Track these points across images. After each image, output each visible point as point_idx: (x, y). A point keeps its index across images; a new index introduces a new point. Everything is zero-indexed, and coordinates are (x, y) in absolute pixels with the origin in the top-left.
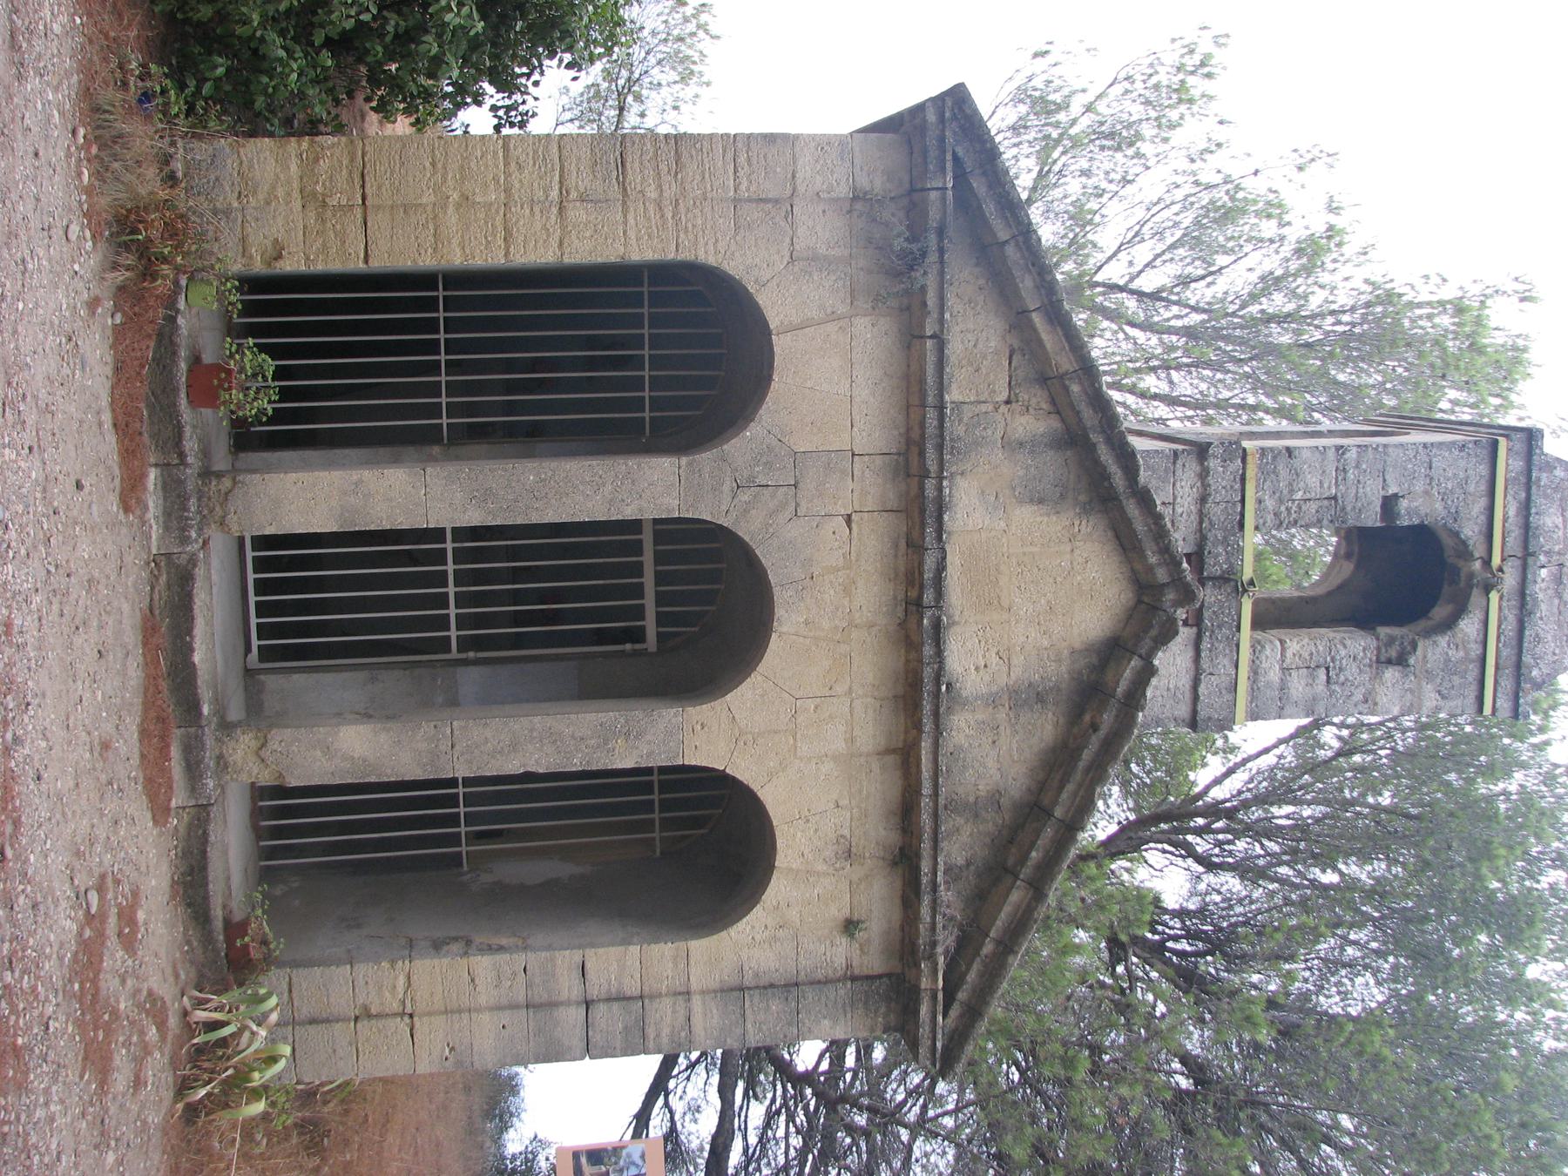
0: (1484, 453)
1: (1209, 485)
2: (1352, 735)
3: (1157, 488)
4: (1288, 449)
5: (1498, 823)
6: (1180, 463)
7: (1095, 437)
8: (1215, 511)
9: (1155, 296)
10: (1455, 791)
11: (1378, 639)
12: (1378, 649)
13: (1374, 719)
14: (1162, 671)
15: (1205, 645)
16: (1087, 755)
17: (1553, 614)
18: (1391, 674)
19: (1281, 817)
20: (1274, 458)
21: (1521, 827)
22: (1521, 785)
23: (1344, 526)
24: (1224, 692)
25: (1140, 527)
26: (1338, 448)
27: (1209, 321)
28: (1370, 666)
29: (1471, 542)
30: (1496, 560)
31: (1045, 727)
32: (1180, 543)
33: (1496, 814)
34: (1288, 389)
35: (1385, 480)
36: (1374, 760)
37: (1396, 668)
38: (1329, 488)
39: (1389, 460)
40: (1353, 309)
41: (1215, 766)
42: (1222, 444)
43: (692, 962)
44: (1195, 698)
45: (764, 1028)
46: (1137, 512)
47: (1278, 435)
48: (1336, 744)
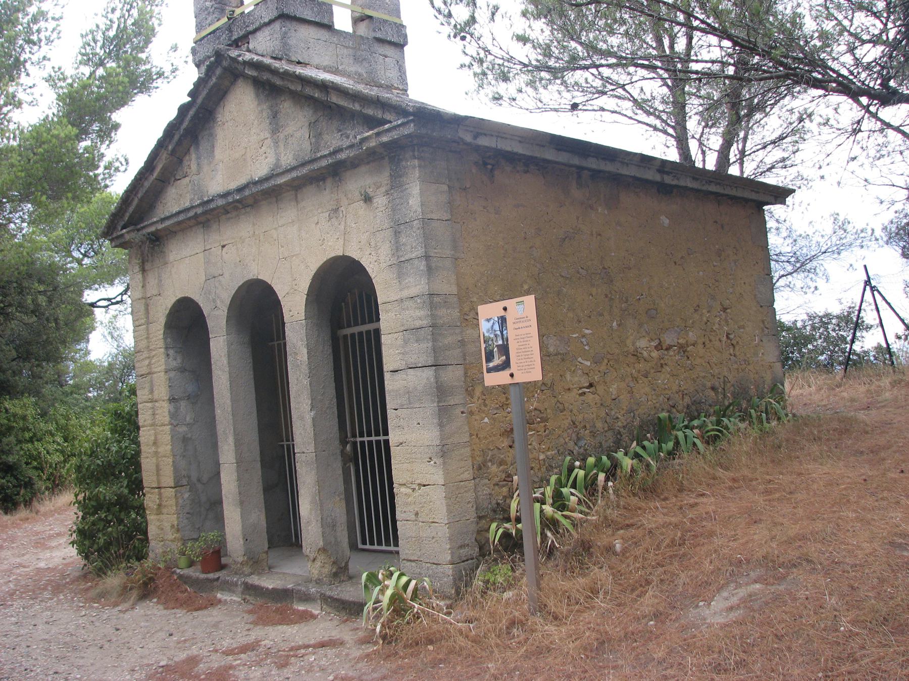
15: (251, 28)
31: (286, 106)
43: (388, 300)
45: (414, 244)
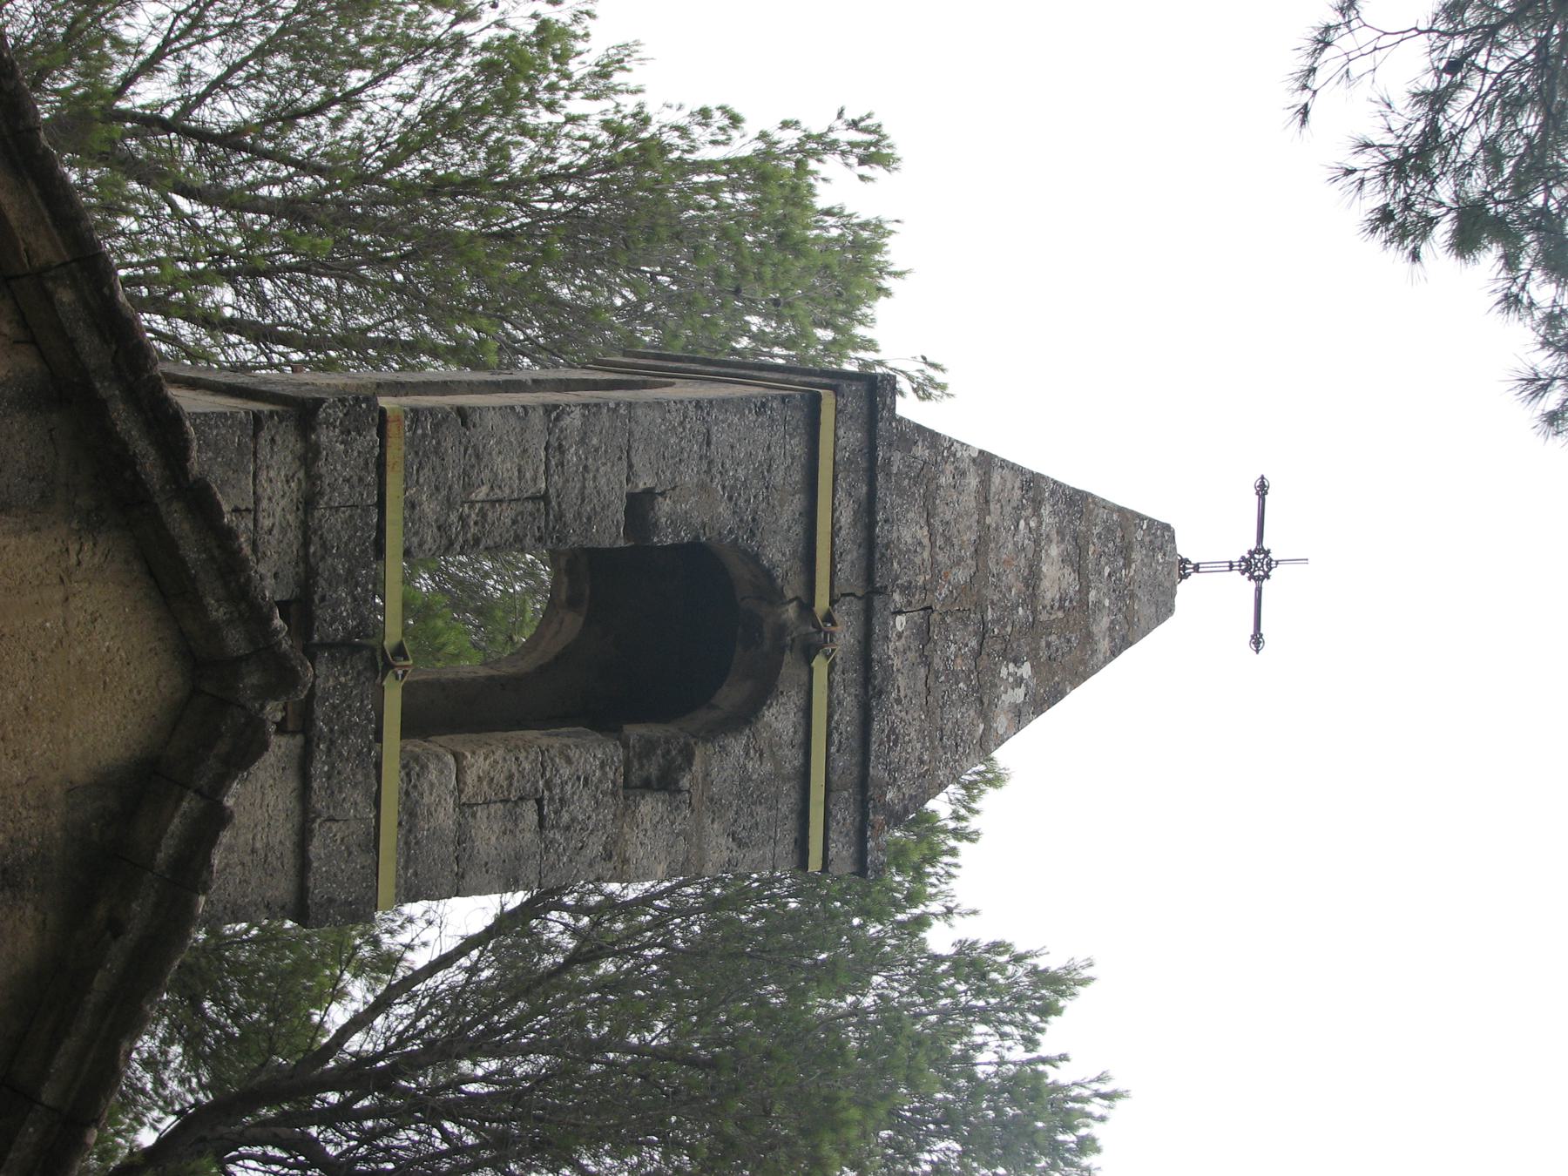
0: (797, 417)
1: (320, 477)
2: (595, 924)
3: (224, 482)
4: (461, 411)
5: (846, 1065)
6: (265, 436)
7: (104, 388)
8: (332, 522)
9: (232, 139)
10: (773, 1015)
11: (626, 746)
12: (627, 764)
13: (633, 892)
14: (240, 818)
15: (319, 767)
16: (101, 982)
17: (916, 693)
18: (649, 807)
19: (475, 1080)
20: (436, 427)
21: (882, 1070)
22: (880, 996)
23: (562, 547)
24: (354, 849)
25: (192, 553)
26: (549, 409)
27: (328, 189)
28: (614, 794)
29: (779, 572)
30: (822, 603)
32: (270, 581)
33: (842, 1047)
34: (468, 315)
35: (630, 466)
36: (637, 967)
37: (660, 796)
38: (535, 479)
39: (637, 430)
40: (581, 174)
41: (359, 993)
42: (342, 401)
44: (303, 865)
46: (186, 526)
47: (445, 387)
48: (569, 943)
